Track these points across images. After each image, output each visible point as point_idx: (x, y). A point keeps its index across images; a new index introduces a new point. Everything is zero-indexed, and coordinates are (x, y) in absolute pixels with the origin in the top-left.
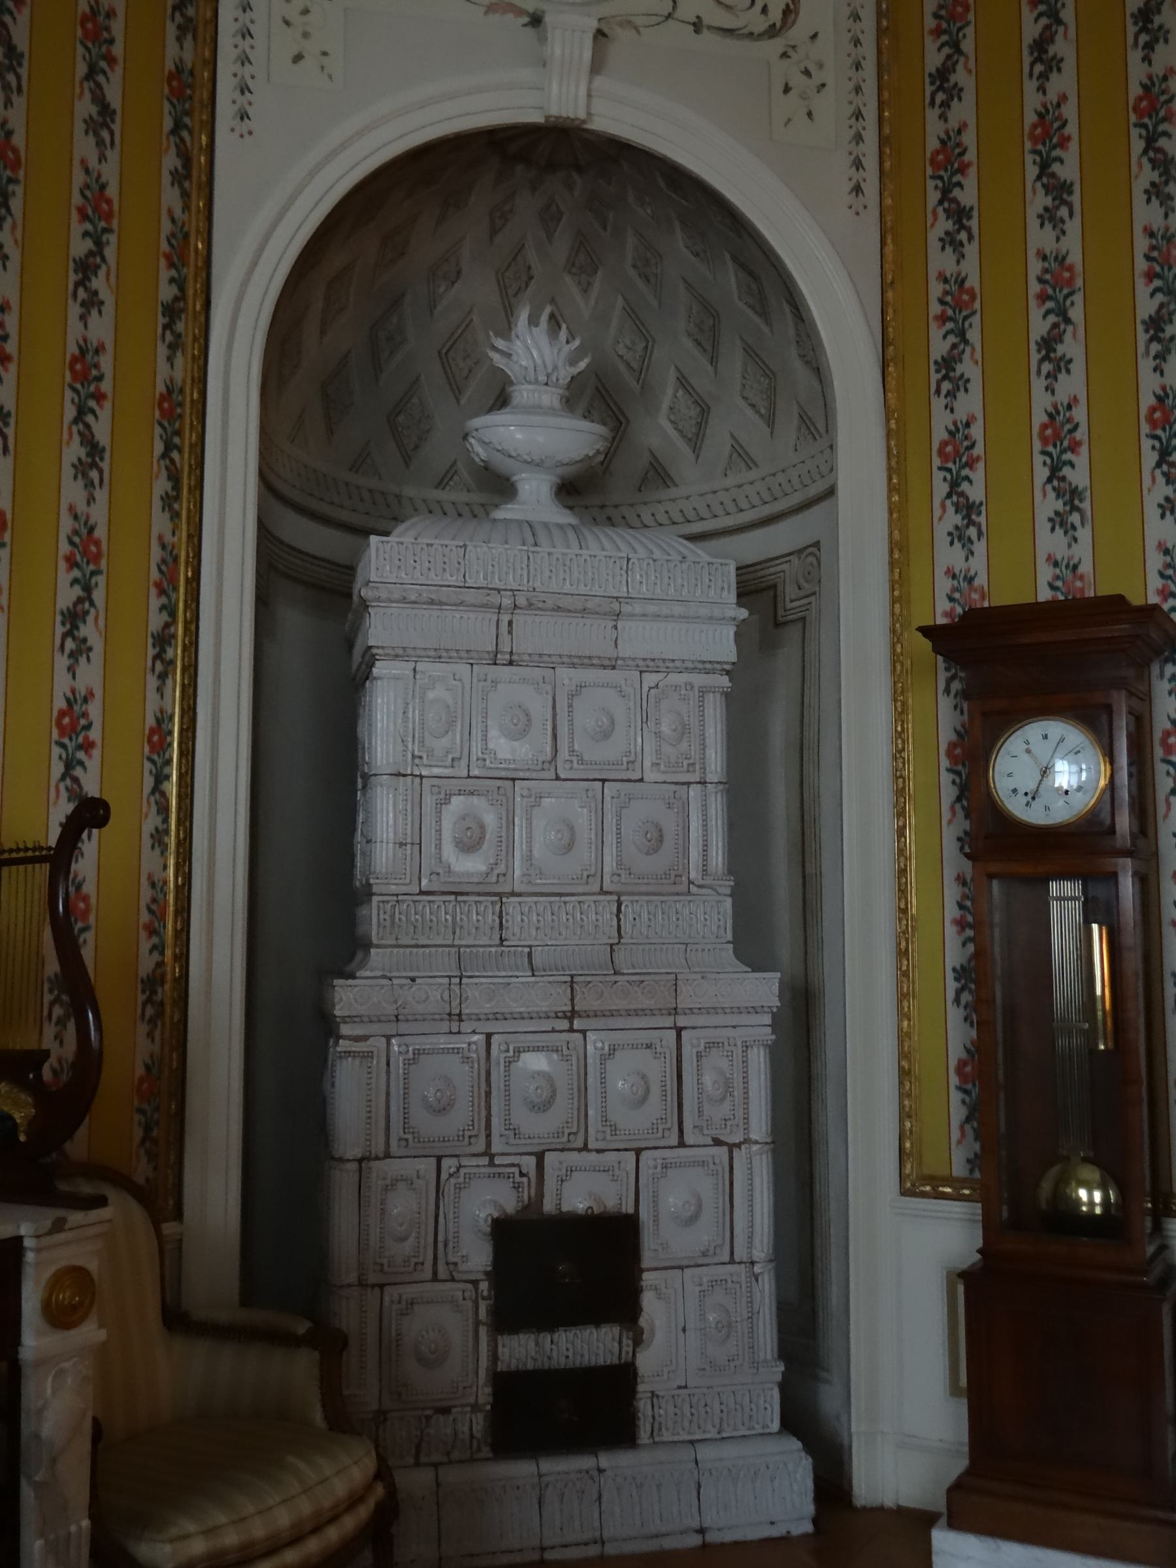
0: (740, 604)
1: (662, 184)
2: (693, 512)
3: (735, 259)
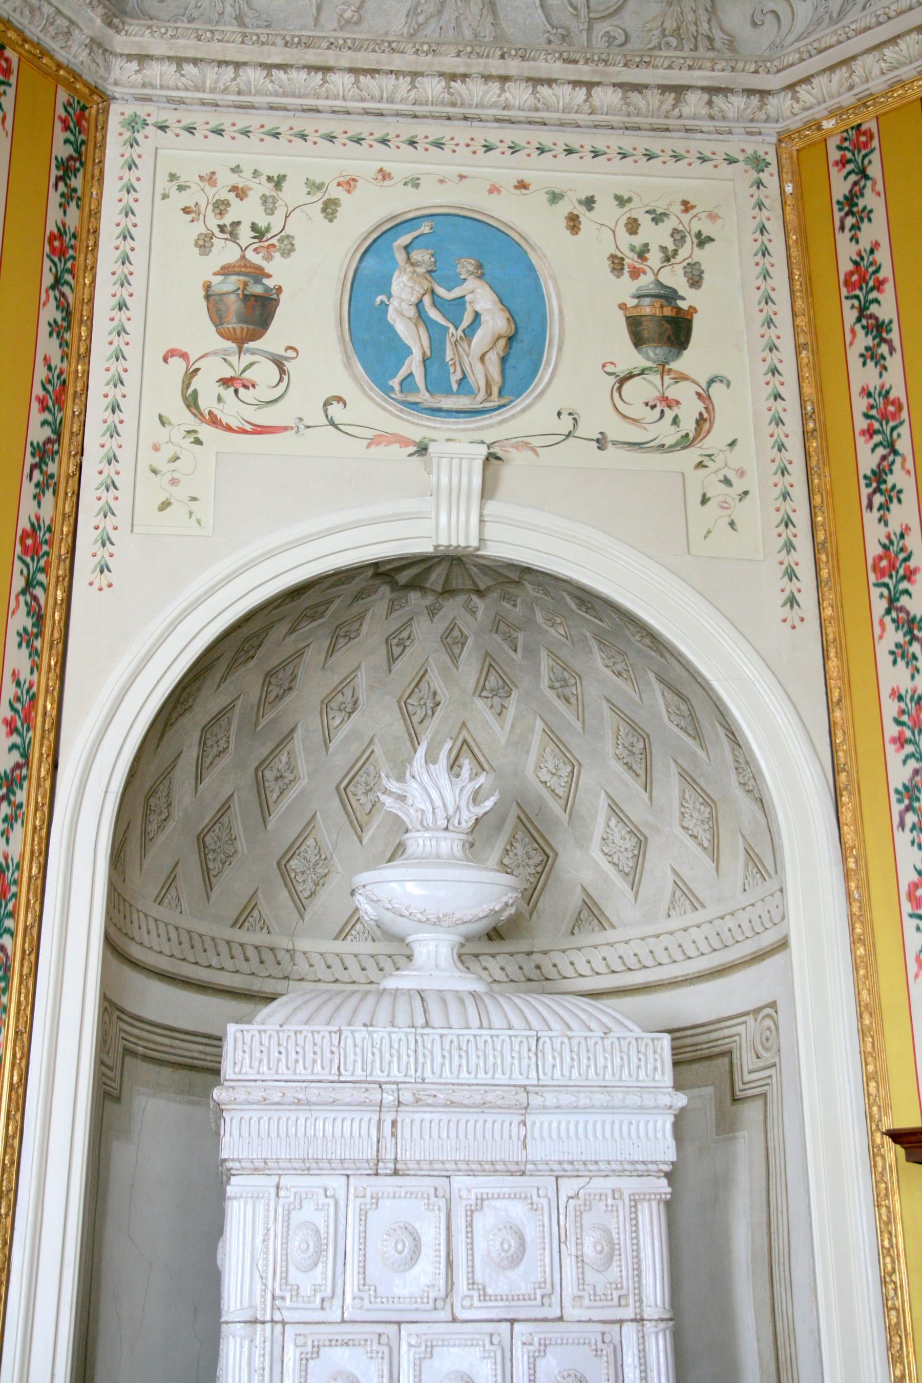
0: (678, 1086)
1: (574, 606)
2: (634, 959)
3: (661, 680)
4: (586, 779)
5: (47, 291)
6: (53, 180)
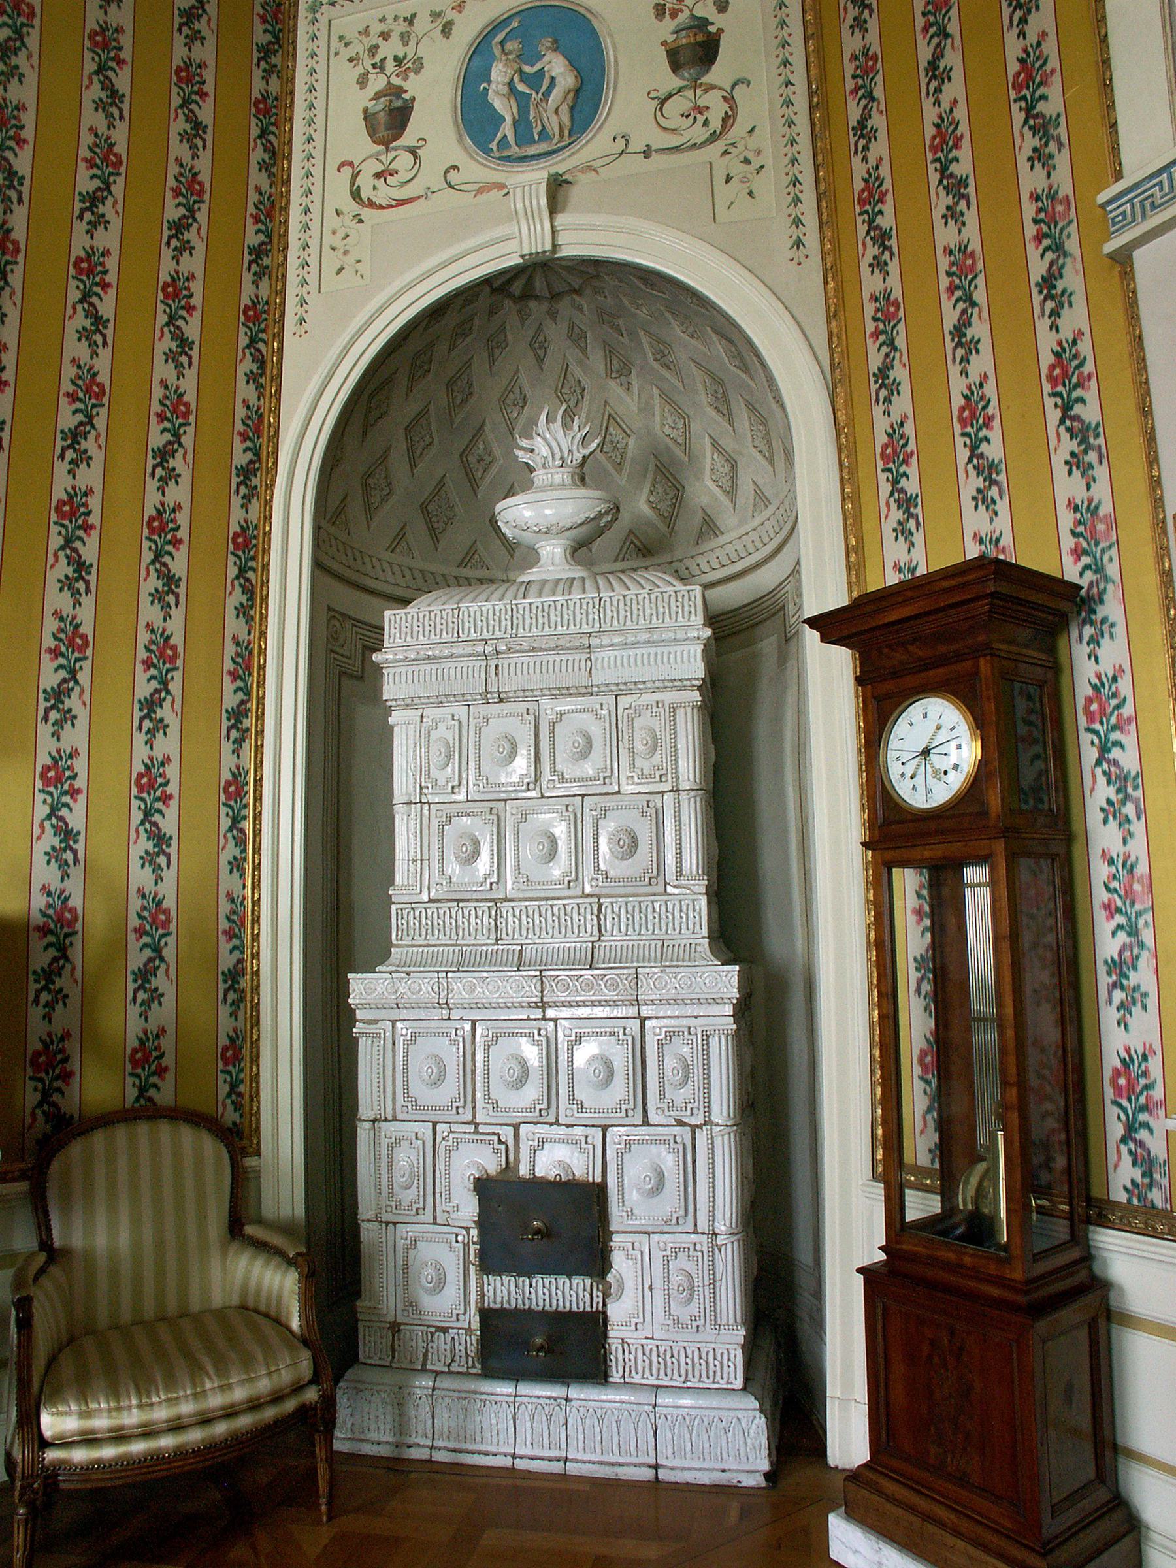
4: (695, 426)
5: (176, 111)
6: (255, 61)
